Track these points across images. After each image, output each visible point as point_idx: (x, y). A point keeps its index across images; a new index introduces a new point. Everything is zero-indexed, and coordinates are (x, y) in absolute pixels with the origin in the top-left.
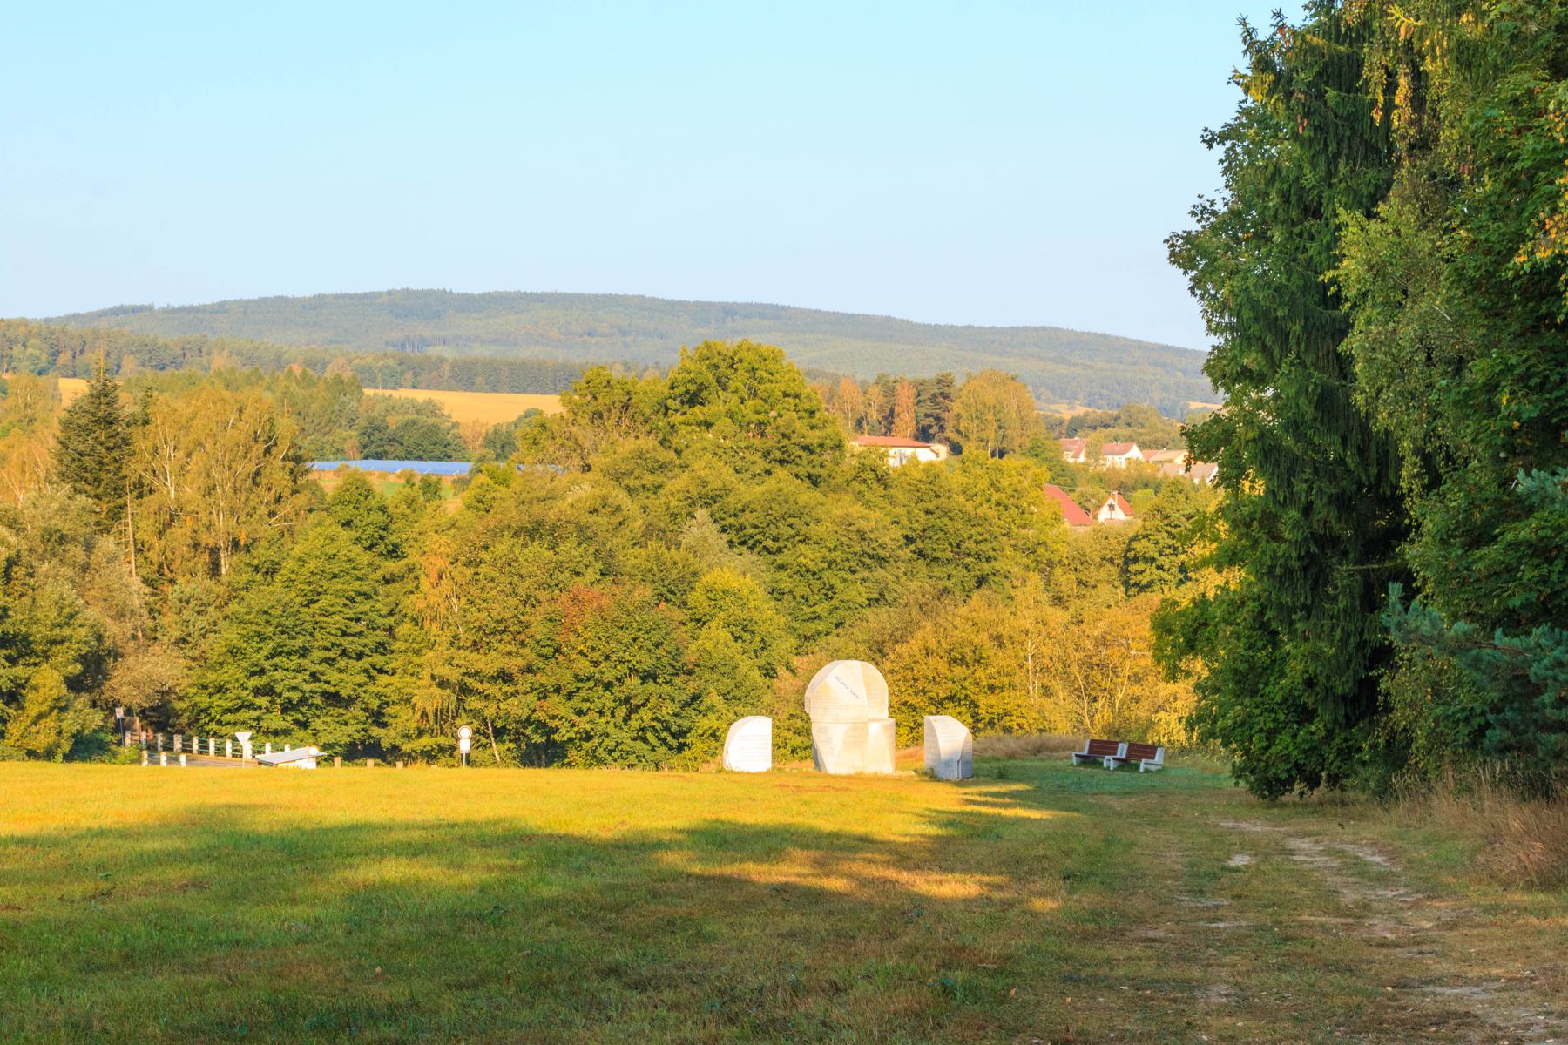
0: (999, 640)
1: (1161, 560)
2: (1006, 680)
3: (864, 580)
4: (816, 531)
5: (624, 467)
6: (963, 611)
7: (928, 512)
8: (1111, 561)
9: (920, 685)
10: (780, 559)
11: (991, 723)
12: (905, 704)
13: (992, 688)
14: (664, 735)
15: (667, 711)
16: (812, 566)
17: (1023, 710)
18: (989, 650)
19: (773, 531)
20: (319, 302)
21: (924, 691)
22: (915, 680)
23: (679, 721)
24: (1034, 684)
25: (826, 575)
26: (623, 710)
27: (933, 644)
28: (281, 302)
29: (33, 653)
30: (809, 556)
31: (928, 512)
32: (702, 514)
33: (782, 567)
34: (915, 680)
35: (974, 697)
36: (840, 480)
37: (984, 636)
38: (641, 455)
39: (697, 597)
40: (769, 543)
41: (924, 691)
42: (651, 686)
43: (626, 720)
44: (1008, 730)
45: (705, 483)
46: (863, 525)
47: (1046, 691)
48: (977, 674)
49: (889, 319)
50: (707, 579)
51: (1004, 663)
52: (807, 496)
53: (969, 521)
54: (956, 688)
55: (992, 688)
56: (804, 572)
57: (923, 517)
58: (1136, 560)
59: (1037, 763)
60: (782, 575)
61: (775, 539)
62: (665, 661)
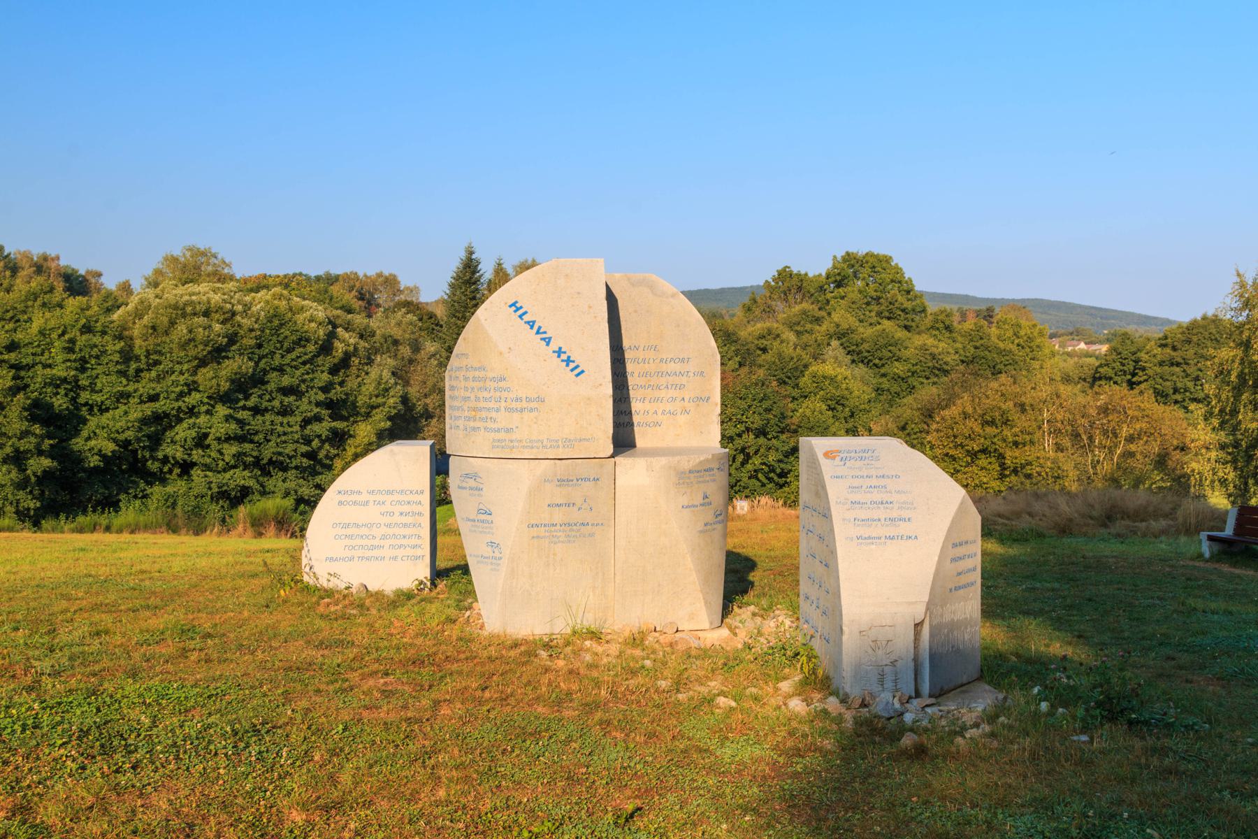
0: (1022, 408)
1: (1116, 378)
2: (1028, 438)
3: (934, 383)
4: (905, 354)
5: (795, 319)
6: (994, 385)
7: (976, 348)
8: (1084, 380)
9: (959, 441)
10: (883, 371)
11: (1015, 471)
12: (947, 455)
13: (1016, 444)
14: (772, 475)
15: (772, 458)
16: (901, 374)
17: (1042, 461)
18: (1014, 415)
19: (879, 354)
20: (722, 291)
21: (962, 446)
22: (955, 437)
23: (782, 465)
24: (1049, 443)
25: (910, 380)
26: (740, 458)
27: (970, 410)
28: (707, 291)
29: (358, 414)
30: (899, 368)
31: (976, 348)
32: (835, 343)
33: (884, 375)
34: (955, 437)
35: (1001, 451)
36: (923, 328)
37: (1011, 404)
38: (804, 312)
39: (805, 381)
40: (877, 361)
41: (962, 446)
42: (762, 440)
43: (743, 464)
44: (1029, 476)
45: (838, 326)
46: (934, 350)
47: (1059, 448)
48: (1005, 433)
49: (967, 296)
50: (812, 369)
51: (1026, 425)
52: (901, 334)
53: (1001, 352)
54: (988, 443)
55: (1016, 444)
56: (897, 378)
57: (972, 350)
58: (1100, 378)
59: (1115, 547)
60: (884, 379)
61: (880, 359)
62: (772, 422)
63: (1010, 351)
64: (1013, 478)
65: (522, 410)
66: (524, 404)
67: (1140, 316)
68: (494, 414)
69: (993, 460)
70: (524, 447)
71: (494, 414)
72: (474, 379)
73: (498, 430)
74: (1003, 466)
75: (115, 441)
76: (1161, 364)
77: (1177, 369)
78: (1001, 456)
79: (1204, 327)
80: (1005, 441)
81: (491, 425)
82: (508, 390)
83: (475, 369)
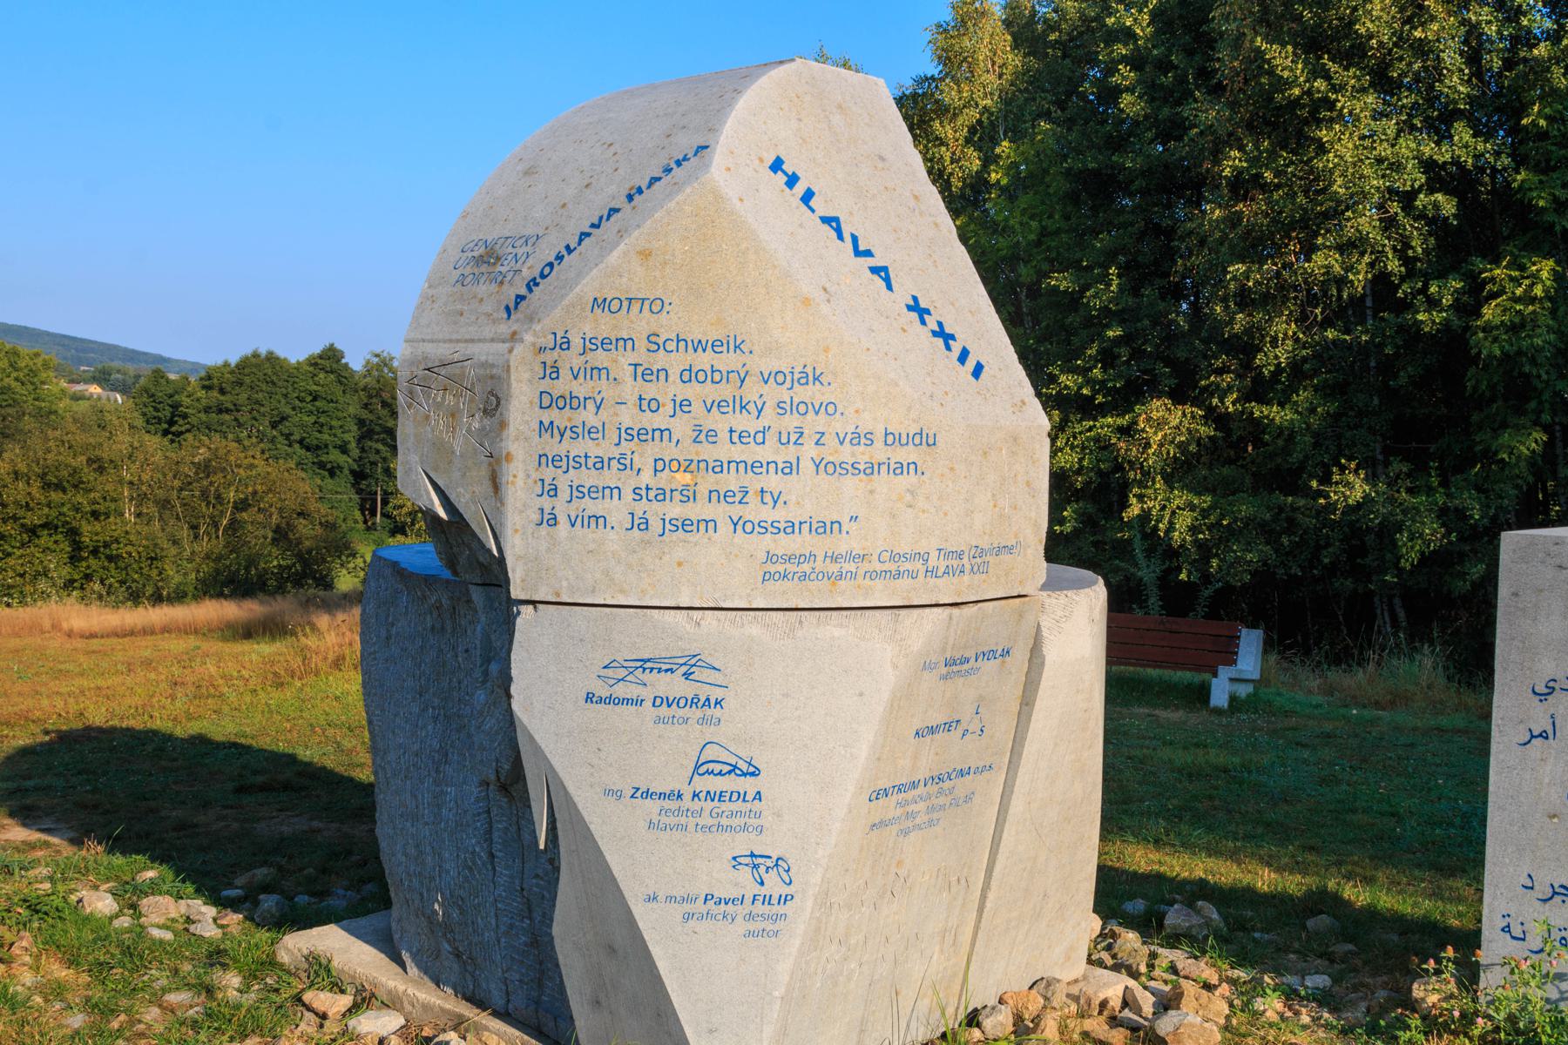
11: (95, 552)
13: (95, 515)
18: (89, 475)
41: (15, 518)
55: (95, 515)
63: (9, 388)
64: (92, 561)
65: (872, 469)
66: (879, 453)
67: (126, 350)
68: (773, 482)
69: (60, 537)
70: (873, 575)
71: (773, 482)
72: (689, 375)
73: (791, 528)
74: (77, 546)
75: (1295, 677)
76: (207, 410)
77: (227, 417)
78: (73, 533)
79: (257, 366)
80: (77, 510)
81: (754, 511)
82: (829, 409)
83: (699, 346)
